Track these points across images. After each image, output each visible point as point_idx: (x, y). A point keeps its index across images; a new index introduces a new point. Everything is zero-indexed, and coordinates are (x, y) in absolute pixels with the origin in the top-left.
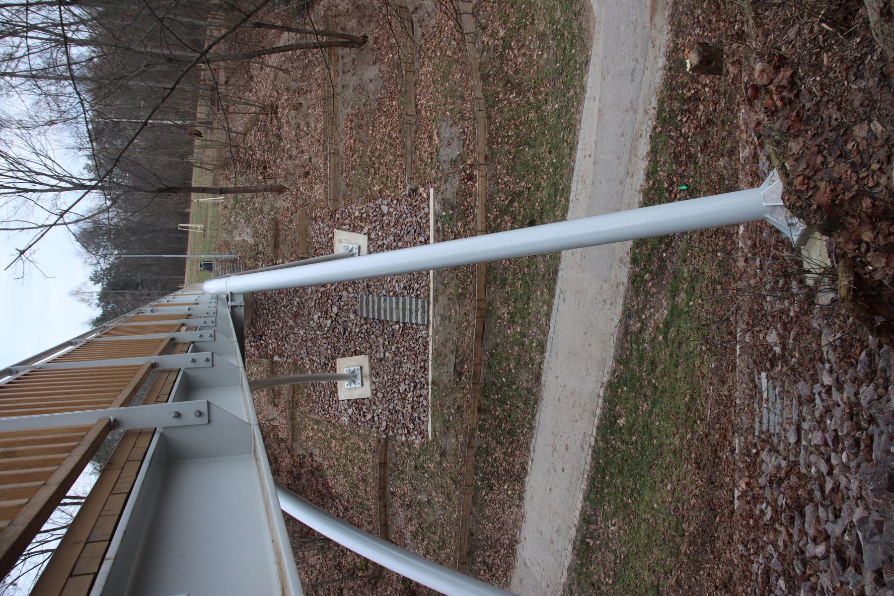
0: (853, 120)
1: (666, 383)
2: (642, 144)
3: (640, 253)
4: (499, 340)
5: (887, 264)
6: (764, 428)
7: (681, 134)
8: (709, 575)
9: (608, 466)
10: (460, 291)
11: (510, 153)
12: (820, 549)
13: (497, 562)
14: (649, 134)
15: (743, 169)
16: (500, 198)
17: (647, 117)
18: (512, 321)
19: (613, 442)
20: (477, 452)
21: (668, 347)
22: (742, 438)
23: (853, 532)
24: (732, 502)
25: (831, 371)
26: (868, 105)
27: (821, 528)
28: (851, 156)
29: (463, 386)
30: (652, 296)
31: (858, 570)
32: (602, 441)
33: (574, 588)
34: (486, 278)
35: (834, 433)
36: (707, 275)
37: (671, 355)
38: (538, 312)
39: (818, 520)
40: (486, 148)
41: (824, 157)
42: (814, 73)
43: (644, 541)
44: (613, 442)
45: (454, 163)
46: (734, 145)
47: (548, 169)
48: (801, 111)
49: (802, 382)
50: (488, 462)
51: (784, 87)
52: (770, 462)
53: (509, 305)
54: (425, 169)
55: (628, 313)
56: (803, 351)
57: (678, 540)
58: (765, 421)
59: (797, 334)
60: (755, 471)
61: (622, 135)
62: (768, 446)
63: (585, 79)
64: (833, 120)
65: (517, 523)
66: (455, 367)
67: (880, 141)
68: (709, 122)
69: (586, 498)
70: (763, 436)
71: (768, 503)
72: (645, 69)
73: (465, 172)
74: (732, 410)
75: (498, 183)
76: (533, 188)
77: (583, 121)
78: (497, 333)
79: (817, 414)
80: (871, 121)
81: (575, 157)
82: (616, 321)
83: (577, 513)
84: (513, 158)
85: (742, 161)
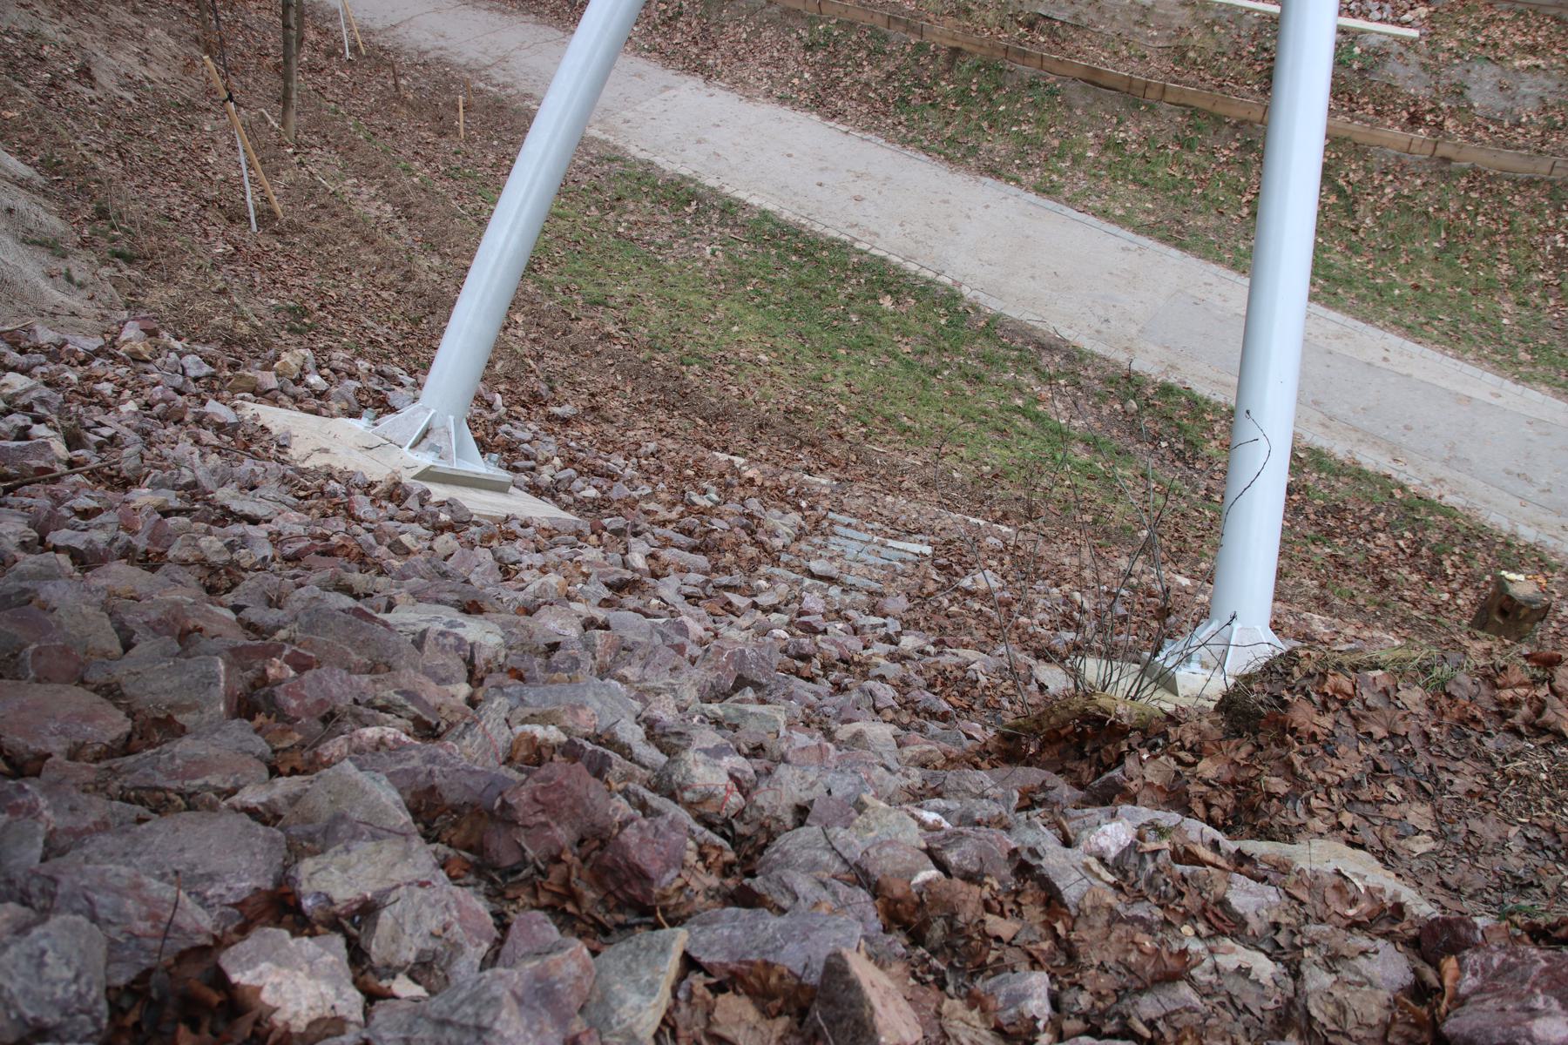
0: (1445, 811)
1: (939, 391)
2: (1378, 458)
3: (1178, 404)
4: (1079, 112)
5: (1150, 785)
6: (837, 528)
7: (1375, 530)
8: (614, 388)
9: (814, 264)
10: (1191, 54)
11: (1440, 210)
12: (638, 560)
13: (678, 38)
14: (1395, 475)
15: (1291, 613)
16: (1355, 171)
17: (1427, 480)
18: (1108, 145)
19: (854, 281)
20: (879, 32)
21: (1001, 411)
22: (827, 491)
23: (662, 613)
24: (725, 449)
25: (922, 652)
26: (1469, 843)
27: (670, 569)
28: (1373, 786)
29: (1007, 26)
30: (1095, 405)
31: (606, 603)
32: (860, 263)
33: (617, 166)
34: (1204, 111)
35: (821, 628)
36: (1111, 506)
37: (985, 413)
38: (1113, 197)
39: (682, 570)
40: (1466, 164)
41: (1381, 741)
42: (1556, 772)
43: (680, 298)
44: (854, 281)
45: (1459, 91)
46: (1336, 611)
47: (1384, 276)
48: (1480, 728)
49: (908, 605)
50: (857, 51)
51: (1539, 712)
52: (782, 523)
53: (1140, 145)
54: (1465, 26)
55: (1074, 356)
56: (960, 620)
57: (675, 353)
58: (850, 532)
59: (990, 619)
60: (771, 497)
61: (1407, 428)
62: (808, 528)
63: (1543, 387)
64: (1452, 777)
65: (738, 85)
66: (1046, 18)
67: (1392, 842)
68: (1384, 584)
69: (765, 215)
70: (825, 523)
71: (717, 504)
72: (1524, 501)
73: (1431, 111)
74: (877, 487)
75: (1386, 174)
76: (1354, 238)
77: (1460, 363)
78: (1093, 111)
79: (851, 613)
80: (1435, 838)
81: (1392, 331)
82: (1066, 333)
83: (742, 195)
84: (1426, 213)
85: (1305, 615)
